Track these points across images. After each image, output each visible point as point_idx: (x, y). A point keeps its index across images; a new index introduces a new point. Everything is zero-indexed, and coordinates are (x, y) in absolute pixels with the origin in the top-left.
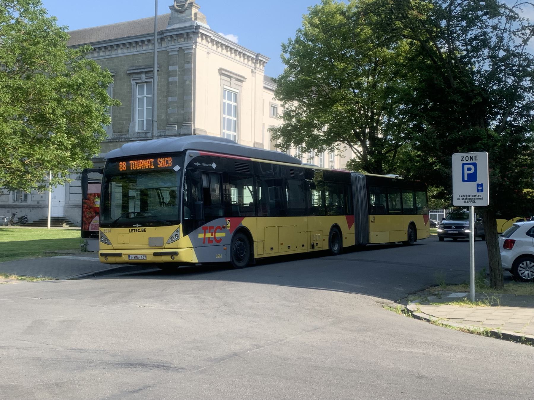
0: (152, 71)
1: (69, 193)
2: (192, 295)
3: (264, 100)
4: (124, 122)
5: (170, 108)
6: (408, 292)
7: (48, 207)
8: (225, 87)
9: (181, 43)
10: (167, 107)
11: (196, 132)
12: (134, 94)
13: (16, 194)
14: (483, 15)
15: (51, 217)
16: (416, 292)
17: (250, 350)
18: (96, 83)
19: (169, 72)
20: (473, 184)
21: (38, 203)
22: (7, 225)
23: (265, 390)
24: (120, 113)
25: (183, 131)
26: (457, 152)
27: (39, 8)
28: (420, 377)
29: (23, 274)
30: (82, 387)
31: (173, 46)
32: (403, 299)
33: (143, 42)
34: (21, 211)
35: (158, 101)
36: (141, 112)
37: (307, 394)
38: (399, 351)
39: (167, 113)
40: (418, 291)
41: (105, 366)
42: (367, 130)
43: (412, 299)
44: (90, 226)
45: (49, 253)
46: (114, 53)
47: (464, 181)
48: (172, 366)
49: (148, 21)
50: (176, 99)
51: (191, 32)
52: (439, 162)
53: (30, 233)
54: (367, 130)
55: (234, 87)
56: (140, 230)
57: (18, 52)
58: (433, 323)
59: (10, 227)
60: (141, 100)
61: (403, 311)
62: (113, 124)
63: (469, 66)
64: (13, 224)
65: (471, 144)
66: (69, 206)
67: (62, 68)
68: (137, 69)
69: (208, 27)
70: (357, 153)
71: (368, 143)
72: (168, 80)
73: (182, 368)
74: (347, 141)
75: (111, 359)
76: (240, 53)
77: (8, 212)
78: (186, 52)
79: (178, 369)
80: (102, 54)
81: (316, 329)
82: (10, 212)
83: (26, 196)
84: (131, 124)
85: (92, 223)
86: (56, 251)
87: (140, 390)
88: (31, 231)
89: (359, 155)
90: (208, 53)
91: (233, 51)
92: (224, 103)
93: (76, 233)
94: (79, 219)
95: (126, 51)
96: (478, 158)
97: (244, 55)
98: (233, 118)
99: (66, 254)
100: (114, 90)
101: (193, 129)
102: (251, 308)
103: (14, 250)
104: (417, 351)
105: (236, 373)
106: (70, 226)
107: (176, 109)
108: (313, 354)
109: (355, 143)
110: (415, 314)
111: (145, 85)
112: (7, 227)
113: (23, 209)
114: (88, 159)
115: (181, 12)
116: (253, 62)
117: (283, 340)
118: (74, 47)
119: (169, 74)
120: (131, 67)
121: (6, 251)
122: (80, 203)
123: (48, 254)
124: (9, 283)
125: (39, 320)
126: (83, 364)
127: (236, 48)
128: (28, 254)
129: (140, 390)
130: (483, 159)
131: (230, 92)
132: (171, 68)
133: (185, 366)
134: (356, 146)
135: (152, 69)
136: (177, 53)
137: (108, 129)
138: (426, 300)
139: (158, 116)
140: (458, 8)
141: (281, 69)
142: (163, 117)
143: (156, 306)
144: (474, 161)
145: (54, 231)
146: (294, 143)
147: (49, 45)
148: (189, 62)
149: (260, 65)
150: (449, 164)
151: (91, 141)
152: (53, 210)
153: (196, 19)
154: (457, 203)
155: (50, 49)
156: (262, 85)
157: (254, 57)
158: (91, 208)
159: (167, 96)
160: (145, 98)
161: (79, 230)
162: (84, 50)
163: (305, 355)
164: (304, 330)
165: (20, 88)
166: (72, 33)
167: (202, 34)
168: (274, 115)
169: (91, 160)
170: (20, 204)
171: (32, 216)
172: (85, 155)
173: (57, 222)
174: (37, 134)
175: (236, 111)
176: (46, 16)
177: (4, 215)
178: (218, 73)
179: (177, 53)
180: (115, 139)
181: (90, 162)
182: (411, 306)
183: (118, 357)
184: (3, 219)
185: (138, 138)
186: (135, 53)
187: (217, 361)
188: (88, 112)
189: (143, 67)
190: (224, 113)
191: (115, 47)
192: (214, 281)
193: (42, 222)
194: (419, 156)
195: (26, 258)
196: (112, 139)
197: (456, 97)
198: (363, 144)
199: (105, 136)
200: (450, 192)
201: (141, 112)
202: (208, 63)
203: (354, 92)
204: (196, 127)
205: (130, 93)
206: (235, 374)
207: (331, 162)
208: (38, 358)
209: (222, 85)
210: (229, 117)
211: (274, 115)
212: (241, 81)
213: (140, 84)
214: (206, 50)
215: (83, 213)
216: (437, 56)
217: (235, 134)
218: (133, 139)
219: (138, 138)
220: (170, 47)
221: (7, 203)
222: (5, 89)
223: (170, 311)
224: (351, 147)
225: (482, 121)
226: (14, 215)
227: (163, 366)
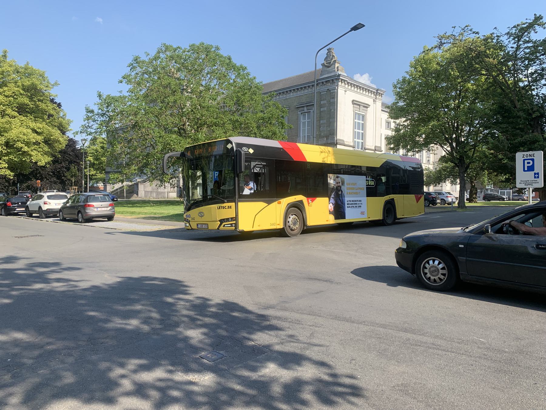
9: (329, 86)
14: (540, 56)
20: (533, 173)
26: (519, 151)
27: (246, 72)
31: (324, 88)
33: (305, 87)
36: (304, 130)
42: (454, 136)
47: (524, 171)
49: (311, 73)
50: (325, 121)
51: (335, 79)
52: (507, 158)
54: (454, 136)
57: (235, 99)
60: (304, 123)
63: (530, 92)
65: (531, 146)
67: (260, 108)
69: (345, 75)
71: (454, 144)
90: (345, 91)
96: (535, 155)
109: (445, 144)
115: (328, 67)
130: (539, 156)
131: (359, 115)
132: (322, 102)
134: (445, 147)
140: (523, 53)
141: (390, 99)
144: (532, 158)
147: (252, 94)
148: (334, 98)
150: (513, 159)
153: (338, 70)
154: (519, 186)
156: (381, 109)
159: (320, 120)
162: (271, 95)
166: (264, 85)
167: (342, 79)
175: (363, 127)
176: (250, 77)
194: (492, 154)
197: (521, 114)
198: (451, 145)
200: (515, 179)
201: (304, 130)
202: (345, 97)
210: (359, 131)
213: (303, 114)
216: (504, 85)
224: (442, 147)
225: (539, 130)
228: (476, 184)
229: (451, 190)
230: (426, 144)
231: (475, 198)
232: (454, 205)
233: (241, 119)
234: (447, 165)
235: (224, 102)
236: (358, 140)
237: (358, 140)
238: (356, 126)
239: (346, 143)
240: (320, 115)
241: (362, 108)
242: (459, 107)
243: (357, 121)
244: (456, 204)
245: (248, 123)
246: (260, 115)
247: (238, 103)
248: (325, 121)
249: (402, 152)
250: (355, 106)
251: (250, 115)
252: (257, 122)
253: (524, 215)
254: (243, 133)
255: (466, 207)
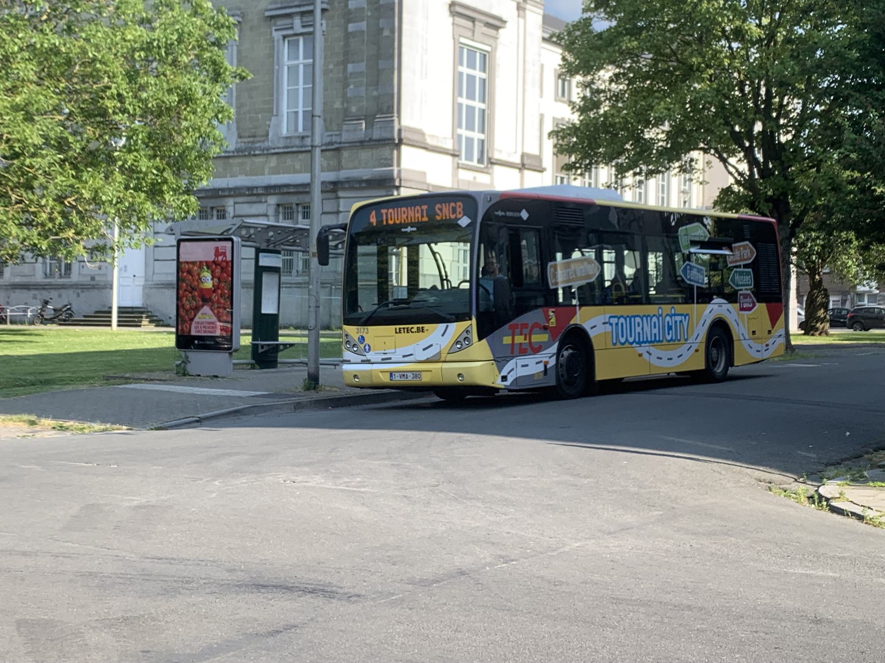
0: (311, 12)
1: (152, 259)
3: (542, 66)
5: (352, 87)
7: (111, 288)
8: (463, 40)
10: (346, 86)
11: (403, 135)
13: (48, 261)
15: (119, 308)
16: (842, 460)
17: (491, 564)
19: (350, 12)
21: (93, 278)
22: (32, 323)
23: (512, 638)
28: (817, 621)
29: (62, 412)
30: (171, 625)
32: (817, 475)
34: (60, 296)
35: (326, 72)
36: (293, 94)
37: (590, 647)
38: (786, 573)
39: (344, 95)
40: (846, 459)
41: (214, 589)
44: (193, 325)
45: (115, 378)
48: (339, 590)
53: (77, 340)
56: (415, 330)
58: (871, 522)
59: (39, 327)
62: (238, 121)
64: (45, 321)
66: (152, 287)
68: (285, 8)
72: (346, 29)
75: (226, 575)
77: (35, 298)
79: (349, 597)
81: (626, 529)
82: (39, 297)
83: (68, 267)
84: (273, 118)
85: (196, 319)
86: (128, 375)
87: (278, 632)
88: (79, 336)
93: (166, 339)
94: (172, 311)
99: (146, 380)
100: (239, 52)
102: (499, 487)
103: (47, 373)
104: (821, 573)
106: (157, 326)
107: (363, 89)
108: (611, 576)
109: (733, 153)
110: (834, 503)
111: (301, 39)
112: (32, 327)
113: (63, 292)
114: (188, 192)
121: (31, 374)
122: (173, 278)
123: (112, 381)
124: (38, 435)
126: (174, 584)
129: (278, 632)
131: (472, 52)
133: (363, 593)
135: (310, 8)
138: (862, 476)
142: (338, 105)
143: (317, 480)
145: (123, 334)
152: (123, 293)
158: (194, 289)
159: (345, 63)
160: (301, 68)
161: (171, 333)
163: (596, 577)
164: (600, 531)
165: (55, 51)
169: (194, 193)
170: (58, 281)
171: (82, 304)
172: (183, 183)
173: (130, 317)
174: (88, 141)
175: (486, 91)
177: (26, 304)
181: (193, 199)
182: (829, 489)
183: (240, 573)
184: (25, 311)
185: (286, 147)
187: (424, 583)
192: (432, 434)
193: (100, 318)
195: (70, 388)
196: (237, 150)
203: (730, 48)
204: (403, 123)
205: (271, 56)
206: (456, 609)
207: (684, 192)
208: (91, 574)
209: (456, 37)
213: (291, 38)
215: (178, 298)
217: (482, 136)
219: (286, 147)
221: (33, 280)
223: (342, 491)
224: (724, 161)
227: (323, 590)
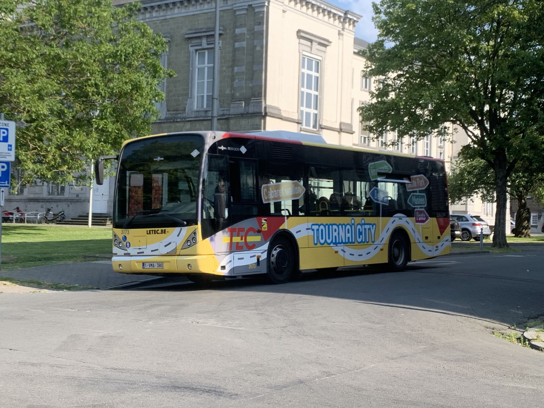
0: (213, 36)
2: (255, 311)
4: (181, 98)
5: (237, 81)
6: (528, 316)
7: (89, 202)
8: (305, 53)
10: (233, 80)
11: (268, 110)
12: (192, 63)
15: (93, 214)
17: (318, 377)
18: (147, 51)
19: (236, 36)
21: (77, 196)
22: (40, 222)
24: (175, 87)
25: (251, 110)
32: (522, 325)
35: (221, 72)
36: (201, 85)
39: (232, 86)
42: (487, 108)
43: (532, 324)
45: (90, 257)
46: (169, 13)
48: (226, 391)
53: (67, 233)
54: (487, 108)
55: (316, 52)
56: (159, 232)
57: (55, 12)
59: (44, 225)
60: (201, 70)
61: (519, 339)
62: (168, 101)
64: (48, 221)
67: (108, 33)
70: (473, 137)
72: (234, 45)
73: (237, 395)
74: (460, 121)
75: (155, 380)
76: (324, 10)
77: (42, 207)
78: (256, 10)
79: (231, 396)
80: (154, 14)
81: (403, 356)
82: (44, 207)
83: (63, 189)
84: (189, 100)
86: (97, 255)
88: (68, 231)
89: (474, 139)
90: (284, 12)
91: (315, 8)
92: (303, 74)
95: (183, 10)
97: (329, 12)
98: (313, 92)
100: (169, 59)
101: (263, 106)
102: (324, 329)
105: (300, 402)
107: (244, 82)
109: (471, 124)
110: (533, 343)
111: (206, 52)
112: (40, 225)
113: (59, 203)
116: (340, 22)
117: (360, 368)
118: (120, 6)
119: (236, 38)
120: (189, 30)
121: (39, 254)
125: (75, 335)
126: (124, 385)
127: (318, 4)
128: (64, 258)
131: (310, 60)
132: (238, 31)
133: (239, 393)
136: (245, 12)
137: (161, 106)
139: (220, 91)
142: (228, 92)
143: (212, 322)
146: (391, 125)
148: (261, 23)
149: (350, 25)
151: (140, 121)
155: (93, 10)
157: (342, 15)
159: (232, 67)
163: (385, 387)
165: (58, 57)
168: (366, 87)
170: (56, 197)
171: (71, 211)
173: (99, 220)
175: (318, 84)
178: (296, 36)
179: (245, 12)
180: (169, 119)
182: (530, 333)
183: (164, 379)
184: (36, 215)
186: (195, 13)
187: (278, 388)
188: (137, 87)
189: (204, 30)
190: (303, 86)
191: (171, 6)
193: (82, 220)
196: (166, 119)
199: (157, 116)
203: (470, 59)
204: (268, 103)
205: (188, 62)
206: (297, 404)
207: (440, 147)
208: (73, 378)
209: (301, 51)
210: (309, 91)
211: (366, 87)
212: (326, 46)
213: (200, 51)
214: (282, 8)
218: (190, 119)
220: (237, 5)
221: (41, 196)
222: (40, 59)
224: (466, 129)
226: (49, 210)
227: (215, 391)
228: (528, 201)
229: (478, 210)
230: (435, 122)
231: (527, 228)
232: (484, 241)
233: (66, 55)
234: (475, 163)
235: (31, 16)
236: (308, 110)
237: (308, 110)
238: (306, 81)
239: (284, 114)
240: (234, 55)
241: (315, 46)
242: (495, 53)
243: (305, 90)
244: (490, 240)
245: (81, 63)
246: (108, 47)
247: (62, 21)
248: (243, 69)
249: (391, 136)
250: (302, 41)
251: (86, 47)
252: (102, 62)
253: (460, 240)
254: (70, 82)
255: (508, 245)
